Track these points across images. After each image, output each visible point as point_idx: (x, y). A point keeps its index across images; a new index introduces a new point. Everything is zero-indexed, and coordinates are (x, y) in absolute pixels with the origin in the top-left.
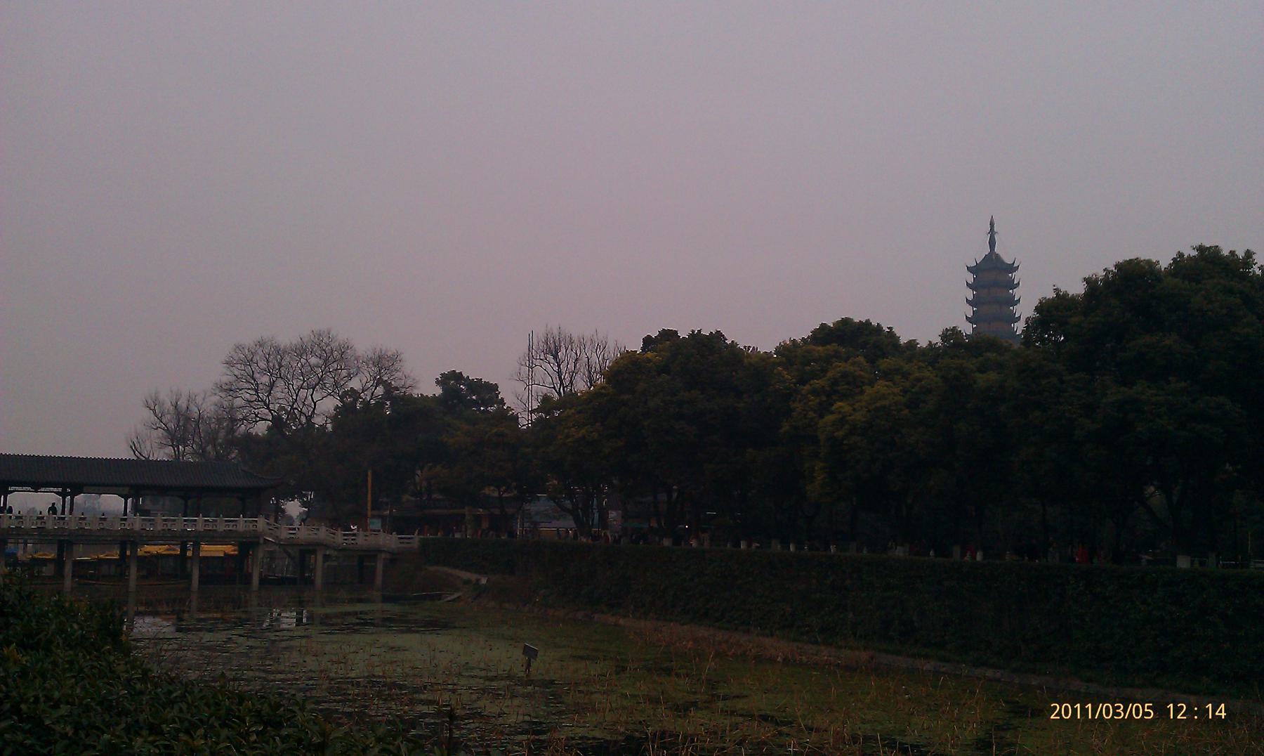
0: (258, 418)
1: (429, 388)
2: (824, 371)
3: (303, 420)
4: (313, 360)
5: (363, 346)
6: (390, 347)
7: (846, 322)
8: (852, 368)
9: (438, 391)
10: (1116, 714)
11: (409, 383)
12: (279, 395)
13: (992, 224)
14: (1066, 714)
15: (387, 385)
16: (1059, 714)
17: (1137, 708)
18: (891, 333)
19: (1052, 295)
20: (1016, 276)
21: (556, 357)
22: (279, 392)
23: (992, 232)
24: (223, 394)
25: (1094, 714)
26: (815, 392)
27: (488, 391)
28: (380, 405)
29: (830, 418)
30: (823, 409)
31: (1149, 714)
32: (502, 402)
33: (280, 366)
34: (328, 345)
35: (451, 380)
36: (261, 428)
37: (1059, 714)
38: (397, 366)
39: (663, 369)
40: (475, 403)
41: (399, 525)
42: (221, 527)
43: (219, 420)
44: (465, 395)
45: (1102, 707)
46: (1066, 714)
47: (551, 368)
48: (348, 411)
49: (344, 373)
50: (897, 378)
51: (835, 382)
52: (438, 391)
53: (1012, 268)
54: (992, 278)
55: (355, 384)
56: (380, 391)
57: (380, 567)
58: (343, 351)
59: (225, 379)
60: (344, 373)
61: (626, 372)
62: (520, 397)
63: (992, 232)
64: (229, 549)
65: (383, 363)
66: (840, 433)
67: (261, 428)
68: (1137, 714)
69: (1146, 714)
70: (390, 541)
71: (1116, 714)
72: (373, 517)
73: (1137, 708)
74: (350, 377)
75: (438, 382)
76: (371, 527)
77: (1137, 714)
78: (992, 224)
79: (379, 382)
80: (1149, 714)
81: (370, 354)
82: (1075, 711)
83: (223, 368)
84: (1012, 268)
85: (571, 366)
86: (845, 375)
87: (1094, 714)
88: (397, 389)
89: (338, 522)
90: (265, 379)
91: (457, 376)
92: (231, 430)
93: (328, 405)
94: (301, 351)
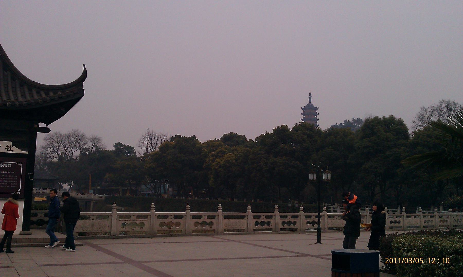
0: (54, 157)
1: (110, 147)
2: (216, 149)
3: (69, 158)
4: (72, 139)
5: (89, 134)
6: (98, 135)
7: (231, 133)
8: (223, 149)
9: (114, 149)
10: (409, 261)
11: (104, 147)
12: (61, 149)
13: (310, 94)
14: (391, 262)
15: (97, 147)
16: (389, 262)
17: (417, 259)
18: (231, 139)
19: (265, 133)
20: (318, 111)
21: (151, 140)
22: (62, 148)
23: (310, 96)
24: (43, 149)
25: (401, 262)
26: (212, 156)
27: (130, 149)
28: (95, 153)
29: (214, 163)
30: (214, 160)
31: (421, 262)
32: (135, 153)
33: (62, 141)
34: (77, 134)
35: (118, 145)
36: (55, 160)
37: (389, 262)
38: (100, 141)
39: (174, 147)
40: (127, 153)
41: (100, 192)
42: (42, 192)
43: (41, 157)
44: (122, 150)
45: (404, 259)
46: (391, 262)
47: (149, 143)
48: (83, 155)
49: (82, 143)
50: (235, 152)
51: (218, 153)
52: (114, 149)
53: (316, 109)
54: (310, 111)
55: (86, 146)
56: (94, 149)
57: (92, 204)
58: (83, 136)
59: (44, 144)
60: (82, 143)
61: (165, 147)
62: (140, 152)
63: (310, 96)
64: (44, 199)
65: (95, 140)
66: (217, 168)
67: (55, 160)
68: (417, 262)
69: (420, 261)
70: (97, 197)
71: (409, 261)
72: (91, 189)
73: (417, 259)
74: (84, 144)
75: (114, 146)
76: (90, 192)
77: (417, 262)
78: (310, 94)
79: (94, 146)
80: (421, 262)
81: (91, 137)
82: (394, 261)
83: (43, 141)
84: (316, 109)
85: (156, 143)
86: (221, 151)
87: (401, 262)
88: (100, 148)
89: (78, 191)
90: (57, 145)
91: (120, 144)
92: (45, 160)
93: (77, 154)
94: (69, 136)
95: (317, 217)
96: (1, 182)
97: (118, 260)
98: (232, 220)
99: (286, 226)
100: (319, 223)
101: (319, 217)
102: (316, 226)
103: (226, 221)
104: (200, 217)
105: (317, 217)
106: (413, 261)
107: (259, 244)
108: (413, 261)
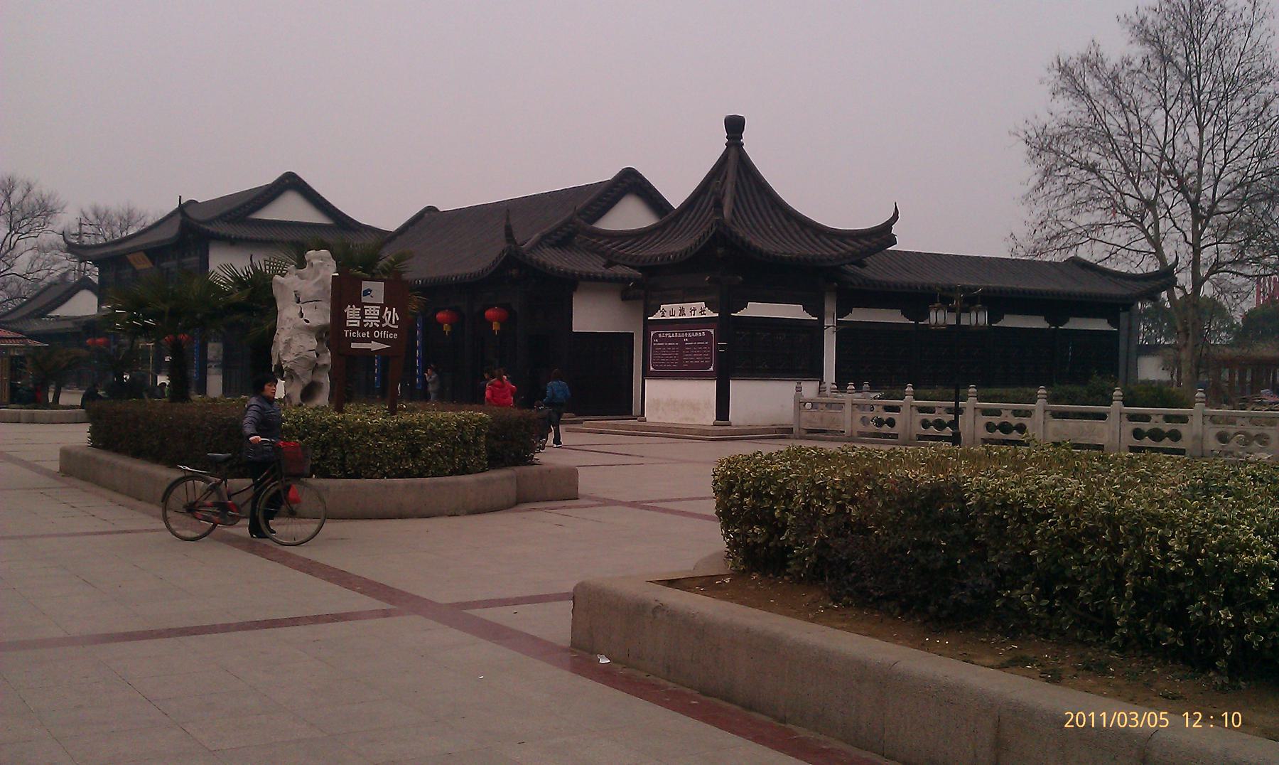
10: (1130, 722)
14: (1081, 723)
16: (1073, 723)
37: (1073, 723)
46: (1081, 723)
68: (1152, 723)
71: (1130, 722)
80: (1164, 722)
82: (1089, 719)
95: (949, 410)
96: (1271, 422)
97: (489, 614)
98: (1071, 423)
99: (933, 431)
100: (954, 424)
101: (957, 411)
102: (948, 431)
103: (1055, 423)
104: (997, 413)
105: (949, 410)
106: (1140, 720)
107: (689, 510)
108: (1140, 720)
